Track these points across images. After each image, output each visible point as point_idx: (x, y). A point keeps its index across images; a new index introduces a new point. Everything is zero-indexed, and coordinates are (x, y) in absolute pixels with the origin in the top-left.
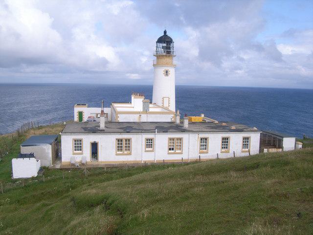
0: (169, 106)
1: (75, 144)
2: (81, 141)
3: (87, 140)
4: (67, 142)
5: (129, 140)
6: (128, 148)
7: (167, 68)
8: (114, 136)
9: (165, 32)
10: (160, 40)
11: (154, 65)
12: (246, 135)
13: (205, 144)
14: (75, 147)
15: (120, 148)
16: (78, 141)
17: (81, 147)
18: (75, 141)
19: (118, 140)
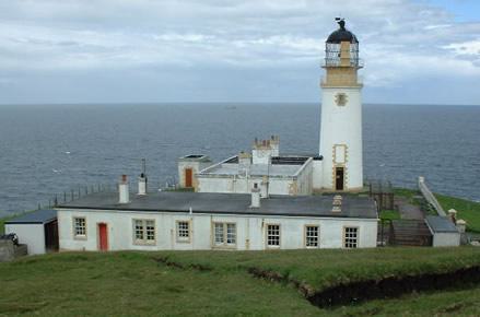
0: (346, 161)
1: (347, 235)
2: (316, 229)
3: (93, 219)
4: (66, 220)
5: (231, 226)
6: (151, 235)
7: (342, 91)
8: (128, 215)
9: (342, 24)
10: (334, 39)
11: (322, 85)
12: (351, 223)
13: (225, 227)
14: (270, 238)
15: (139, 233)
16: (312, 228)
17: (278, 238)
18: (308, 228)
19: (347, 229)
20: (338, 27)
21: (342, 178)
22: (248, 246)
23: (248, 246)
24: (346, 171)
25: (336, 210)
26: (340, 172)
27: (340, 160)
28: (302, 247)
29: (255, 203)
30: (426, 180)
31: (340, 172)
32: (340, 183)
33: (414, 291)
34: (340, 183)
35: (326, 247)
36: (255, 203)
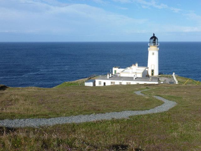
9: (154, 35)
26: (153, 71)
28: (110, 85)
29: (134, 79)
31: (153, 71)
32: (152, 74)
34: (152, 74)
36: (134, 79)
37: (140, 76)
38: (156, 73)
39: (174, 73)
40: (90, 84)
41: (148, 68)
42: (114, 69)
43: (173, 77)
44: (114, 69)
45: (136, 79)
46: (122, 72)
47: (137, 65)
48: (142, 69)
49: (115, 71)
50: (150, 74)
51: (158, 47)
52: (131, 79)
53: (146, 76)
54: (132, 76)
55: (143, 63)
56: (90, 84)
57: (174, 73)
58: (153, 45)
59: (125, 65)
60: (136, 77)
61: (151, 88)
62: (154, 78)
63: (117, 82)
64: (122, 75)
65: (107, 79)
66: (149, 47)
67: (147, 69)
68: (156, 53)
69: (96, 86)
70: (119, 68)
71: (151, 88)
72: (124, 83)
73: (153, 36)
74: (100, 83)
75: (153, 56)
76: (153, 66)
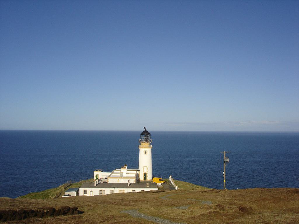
0: (147, 171)
9: (145, 129)
20: (144, 130)
21: (146, 177)
22: (90, 195)
23: (90, 195)
24: (147, 174)
25: (148, 183)
26: (145, 175)
27: (145, 171)
28: (99, 195)
29: (129, 185)
30: (174, 188)
31: (145, 175)
32: (145, 178)
33: (126, 167)
34: (145, 178)
35: (115, 193)
36: (129, 185)
37: (133, 181)
38: (149, 177)
39: (171, 177)
40: (73, 194)
41: (139, 171)
42: (95, 173)
43: (169, 181)
44: (95, 173)
45: (97, 185)
46: (110, 176)
47: (126, 167)
48: (133, 173)
49: (97, 176)
50: (142, 178)
51: (151, 144)
52: (124, 185)
53: (138, 183)
54: (126, 182)
55: (134, 165)
56: (73, 194)
57: (171, 177)
58: (145, 142)
59: (110, 168)
60: (97, 183)
61: (149, 195)
62: (152, 184)
63: (108, 191)
64: (110, 181)
65: (95, 187)
66: (140, 144)
67: (138, 172)
68: (149, 151)
69: (80, 195)
70: (102, 172)
71: (149, 195)
72: (116, 190)
73: (144, 130)
74: (85, 192)
75: (145, 155)
76: (145, 168)
